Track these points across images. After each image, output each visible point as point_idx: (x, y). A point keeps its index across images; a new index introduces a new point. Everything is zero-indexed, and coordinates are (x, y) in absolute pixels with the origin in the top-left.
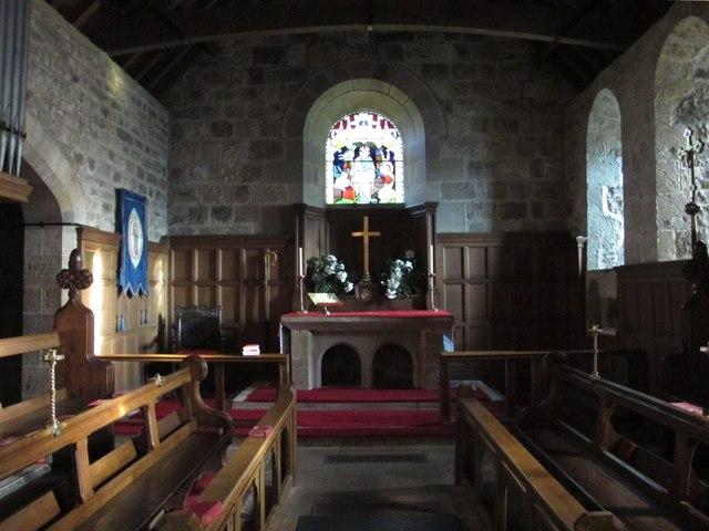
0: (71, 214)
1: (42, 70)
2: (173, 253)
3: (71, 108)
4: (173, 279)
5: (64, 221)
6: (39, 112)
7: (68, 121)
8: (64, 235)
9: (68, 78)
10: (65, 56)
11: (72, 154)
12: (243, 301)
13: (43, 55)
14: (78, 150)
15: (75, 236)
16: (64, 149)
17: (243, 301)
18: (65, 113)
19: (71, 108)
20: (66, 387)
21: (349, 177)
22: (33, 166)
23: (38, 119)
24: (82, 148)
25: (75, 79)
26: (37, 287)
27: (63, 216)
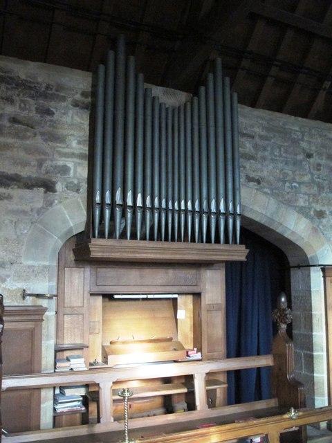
0: (316, 257)
1: (272, 159)
2: (132, 59)
3: (307, 178)
4: (272, 403)
5: (311, 264)
6: (272, 190)
7: (304, 189)
8: (311, 275)
9: (300, 157)
10: (295, 142)
11: (312, 213)
12: (197, 221)
13: (272, 149)
14: (318, 208)
15: (321, 274)
16: (303, 211)
17: (197, 221)
18: (300, 183)
19: (307, 178)
20: (278, 397)
21: (55, 409)
22: (274, 229)
23: (272, 195)
24: (323, 205)
25: (309, 156)
26: (299, 313)
27: (310, 261)
